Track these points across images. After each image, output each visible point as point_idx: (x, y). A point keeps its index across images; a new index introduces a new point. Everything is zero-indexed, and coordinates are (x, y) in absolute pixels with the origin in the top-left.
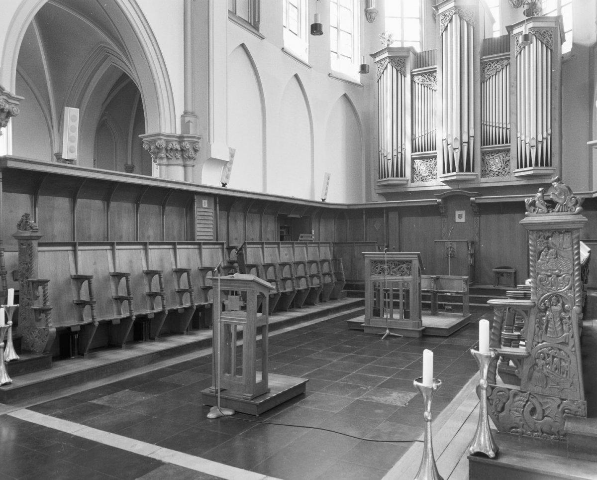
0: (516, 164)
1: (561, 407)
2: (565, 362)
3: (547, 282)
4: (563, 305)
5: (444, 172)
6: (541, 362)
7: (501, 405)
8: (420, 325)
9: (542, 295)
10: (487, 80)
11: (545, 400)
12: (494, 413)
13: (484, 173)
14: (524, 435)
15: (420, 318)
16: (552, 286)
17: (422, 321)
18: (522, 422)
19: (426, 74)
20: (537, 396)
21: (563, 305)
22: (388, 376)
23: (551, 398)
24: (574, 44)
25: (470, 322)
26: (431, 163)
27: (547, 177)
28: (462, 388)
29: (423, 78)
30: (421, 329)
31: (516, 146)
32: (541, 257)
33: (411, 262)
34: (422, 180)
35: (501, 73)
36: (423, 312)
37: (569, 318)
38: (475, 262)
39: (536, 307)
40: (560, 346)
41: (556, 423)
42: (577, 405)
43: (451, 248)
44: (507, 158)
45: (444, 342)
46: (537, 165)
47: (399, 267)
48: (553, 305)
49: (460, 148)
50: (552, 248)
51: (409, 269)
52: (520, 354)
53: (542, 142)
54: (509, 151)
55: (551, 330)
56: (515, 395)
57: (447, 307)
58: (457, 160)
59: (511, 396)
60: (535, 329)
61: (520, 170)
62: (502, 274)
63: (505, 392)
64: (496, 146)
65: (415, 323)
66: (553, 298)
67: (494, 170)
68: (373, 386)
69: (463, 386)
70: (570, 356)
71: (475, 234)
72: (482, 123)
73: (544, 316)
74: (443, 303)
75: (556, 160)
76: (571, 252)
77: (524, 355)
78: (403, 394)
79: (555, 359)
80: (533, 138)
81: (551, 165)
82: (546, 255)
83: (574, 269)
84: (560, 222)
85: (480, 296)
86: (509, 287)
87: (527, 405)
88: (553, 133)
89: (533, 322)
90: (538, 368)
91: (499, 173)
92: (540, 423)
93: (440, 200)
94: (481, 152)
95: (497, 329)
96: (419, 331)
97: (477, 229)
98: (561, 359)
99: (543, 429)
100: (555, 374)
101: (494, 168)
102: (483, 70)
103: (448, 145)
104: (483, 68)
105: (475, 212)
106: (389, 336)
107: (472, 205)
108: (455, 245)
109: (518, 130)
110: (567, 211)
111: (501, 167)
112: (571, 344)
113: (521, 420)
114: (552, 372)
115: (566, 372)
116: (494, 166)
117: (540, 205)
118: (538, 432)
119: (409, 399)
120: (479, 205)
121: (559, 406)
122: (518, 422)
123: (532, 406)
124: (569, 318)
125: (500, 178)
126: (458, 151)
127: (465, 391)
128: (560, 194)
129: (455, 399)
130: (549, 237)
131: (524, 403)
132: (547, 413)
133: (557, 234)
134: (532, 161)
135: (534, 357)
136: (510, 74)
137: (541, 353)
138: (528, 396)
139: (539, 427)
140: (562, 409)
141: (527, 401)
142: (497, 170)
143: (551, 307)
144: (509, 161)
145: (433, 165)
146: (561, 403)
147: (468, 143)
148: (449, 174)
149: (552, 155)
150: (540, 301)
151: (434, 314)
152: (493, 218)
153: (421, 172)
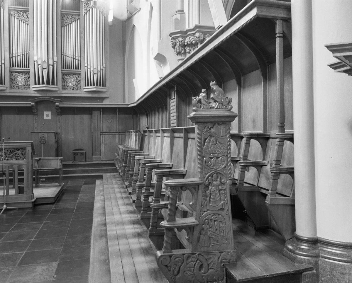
0: (85, 83)
4: (221, 179)
5: (35, 84)
6: (205, 227)
7: (177, 269)
9: (207, 174)
10: (65, 26)
11: (209, 257)
12: (171, 277)
13: (64, 87)
15: (32, 191)
16: (214, 166)
17: (33, 194)
18: (193, 279)
19: (21, 11)
20: (204, 255)
21: (221, 179)
22: (24, 250)
23: (213, 253)
24: (114, 17)
27: (103, 93)
28: (90, 246)
29: (19, 14)
30: (33, 200)
32: (206, 144)
33: (25, 149)
34: (19, 88)
35: (74, 23)
37: (225, 189)
38: (58, 146)
40: (220, 212)
41: (217, 272)
43: (43, 137)
45: (53, 207)
46: (97, 85)
47: (15, 153)
48: (214, 181)
49: (47, 68)
50: (214, 136)
54: (80, 74)
56: (188, 257)
57: (41, 179)
58: (45, 77)
59: (185, 259)
62: (77, 154)
63: (180, 258)
64: (76, 70)
65: (29, 196)
67: (71, 86)
68: (14, 265)
71: (58, 128)
72: (62, 53)
73: (208, 190)
78: (46, 267)
79: (215, 223)
80: (95, 68)
81: (105, 86)
84: (221, 116)
87: (197, 263)
88: (106, 67)
90: (204, 232)
91: (74, 88)
92: (206, 275)
93: (33, 104)
94: (62, 73)
97: (59, 125)
98: (219, 221)
101: (70, 84)
102: (62, 19)
103: (38, 65)
104: (62, 18)
105: (58, 113)
106: (6, 210)
107: (56, 108)
108: (46, 135)
109: (86, 62)
110: (223, 108)
111: (75, 84)
114: (214, 233)
115: (222, 231)
116: (70, 83)
117: (205, 102)
119: (55, 270)
120: (62, 108)
121: (219, 258)
123: (201, 263)
125: (74, 91)
126: (46, 70)
131: (195, 263)
132: (211, 266)
136: (80, 25)
141: (197, 260)
142: (72, 86)
144: (80, 81)
145: (27, 78)
146: (220, 255)
147: (53, 66)
149: (106, 80)
152: (70, 117)
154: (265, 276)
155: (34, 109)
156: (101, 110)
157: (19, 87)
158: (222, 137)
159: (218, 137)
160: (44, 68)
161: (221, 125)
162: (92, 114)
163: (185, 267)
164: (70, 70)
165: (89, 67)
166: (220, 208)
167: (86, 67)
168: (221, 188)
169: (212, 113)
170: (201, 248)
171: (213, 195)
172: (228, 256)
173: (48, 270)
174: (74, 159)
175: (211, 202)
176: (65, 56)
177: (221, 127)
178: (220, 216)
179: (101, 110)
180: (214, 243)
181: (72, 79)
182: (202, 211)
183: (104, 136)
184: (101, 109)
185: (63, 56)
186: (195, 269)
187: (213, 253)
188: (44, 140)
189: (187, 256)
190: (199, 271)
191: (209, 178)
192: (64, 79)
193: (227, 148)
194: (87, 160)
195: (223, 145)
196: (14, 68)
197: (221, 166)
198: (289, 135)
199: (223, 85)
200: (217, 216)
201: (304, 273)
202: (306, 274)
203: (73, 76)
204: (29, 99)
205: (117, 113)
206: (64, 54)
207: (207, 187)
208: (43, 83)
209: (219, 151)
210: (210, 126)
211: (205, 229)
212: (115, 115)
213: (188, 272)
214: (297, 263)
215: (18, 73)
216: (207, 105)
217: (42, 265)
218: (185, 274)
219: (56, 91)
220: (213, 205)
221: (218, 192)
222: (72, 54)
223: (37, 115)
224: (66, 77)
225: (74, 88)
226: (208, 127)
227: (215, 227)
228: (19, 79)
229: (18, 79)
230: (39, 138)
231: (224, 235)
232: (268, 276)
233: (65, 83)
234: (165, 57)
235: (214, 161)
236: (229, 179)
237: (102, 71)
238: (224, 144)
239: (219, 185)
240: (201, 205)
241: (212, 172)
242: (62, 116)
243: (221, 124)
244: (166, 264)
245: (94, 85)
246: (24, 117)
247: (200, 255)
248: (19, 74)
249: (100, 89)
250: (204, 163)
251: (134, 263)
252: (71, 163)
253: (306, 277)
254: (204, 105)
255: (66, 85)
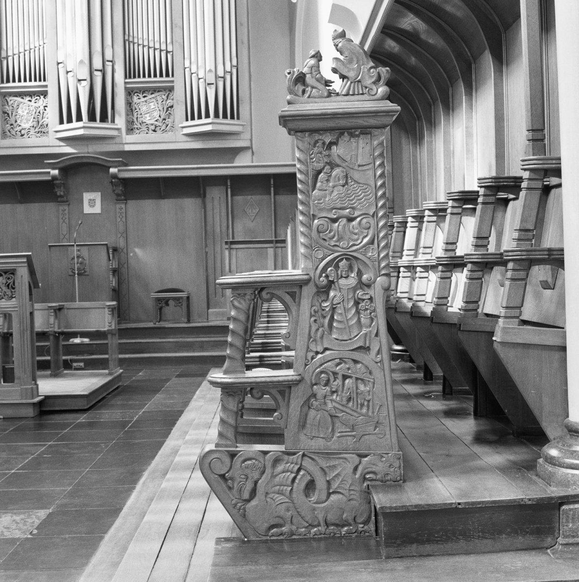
1: (360, 468)
2: (365, 386)
3: (330, 232)
4: (360, 274)
5: (61, 122)
6: (321, 391)
7: (249, 486)
8: (35, 392)
9: (323, 259)
11: (332, 463)
12: (236, 505)
14: (294, 537)
16: (339, 240)
17: (37, 385)
18: (289, 513)
20: (316, 458)
21: (360, 274)
25: (120, 384)
26: (37, 105)
28: (134, 488)
31: (184, 79)
32: (319, 184)
33: (13, 272)
36: (39, 373)
37: (371, 299)
38: (119, 283)
39: (311, 284)
40: (357, 356)
42: (386, 461)
43: (78, 257)
44: (169, 102)
45: (82, 418)
46: (217, 115)
48: (342, 277)
49: (89, 80)
50: (338, 166)
51: (11, 286)
52: (286, 378)
53: (224, 78)
54: (171, 89)
55: (340, 326)
56: (277, 461)
59: (269, 465)
60: (310, 327)
61: (190, 123)
62: (166, 301)
64: (155, 79)
65: (26, 389)
66: (341, 264)
67: (148, 122)
69: (136, 484)
70: (373, 370)
71: (119, 235)
72: (127, 38)
73: (326, 301)
74: (69, 357)
75: (244, 111)
76: (371, 173)
77: (292, 381)
78: (22, 516)
79: (347, 381)
80: (210, 71)
81: (238, 118)
82: (328, 181)
83: (377, 206)
85: (134, 341)
86: (178, 323)
87: (299, 477)
89: (308, 314)
90: (317, 403)
93: (56, 172)
95: (239, 335)
96: (34, 404)
98: (357, 379)
99: (328, 518)
100: (348, 411)
101: (147, 119)
103: (68, 72)
107: (112, 182)
108: (85, 252)
109: (186, 56)
110: (363, 94)
111: (160, 116)
112: (375, 348)
113: (288, 510)
114: (343, 405)
115: (366, 403)
118: (319, 525)
119: (37, 522)
120: (126, 182)
121: (356, 469)
122: (282, 513)
124: (371, 299)
126: (86, 85)
127: (140, 492)
128: (350, 61)
129: (125, 509)
130: (331, 144)
131: (293, 475)
132: (335, 486)
133: (346, 137)
134: (210, 111)
135: (309, 382)
137: (322, 372)
138: (299, 460)
139: (321, 517)
140: (361, 475)
141: (299, 470)
142: (152, 122)
143: (337, 281)
144: (172, 107)
145: (42, 108)
146: (360, 463)
147: (103, 72)
148: (70, 126)
149: (240, 102)
150: (318, 271)
151: (55, 375)
153: (18, 122)
154: (452, 504)
155: (58, 187)
156: (229, 184)
157: (23, 132)
158: (360, 168)
159: (351, 166)
160: (79, 80)
161: (358, 136)
162: (205, 196)
163: (267, 484)
164: (147, 79)
165: (194, 70)
166: (358, 345)
167: (187, 70)
168: (359, 296)
169: (329, 106)
170: (309, 440)
171: (340, 312)
172: (380, 464)
173: (25, 521)
174: (160, 314)
175: (335, 330)
176: (134, 44)
177: (358, 142)
178: (359, 366)
179: (229, 184)
180: (342, 432)
181: (152, 104)
182: (311, 351)
183: (234, 252)
184: (229, 181)
185: (134, 45)
186: (294, 490)
187: (340, 456)
188: (81, 263)
189: (274, 457)
190: (307, 496)
191: (329, 269)
192: (130, 106)
193: (376, 194)
194: (194, 316)
195: (365, 187)
196: (11, 84)
197: (359, 241)
198: (554, 162)
199: (473, 66)
200: (351, 364)
201: (565, 507)
202: (570, 510)
203: (153, 96)
204: (45, 161)
205: (272, 189)
206: (131, 39)
207: (324, 291)
208: (79, 118)
209: (354, 201)
210: (327, 141)
211: (319, 396)
212: (269, 196)
213: (277, 495)
214: (557, 486)
215: (20, 96)
216: (321, 86)
217: (15, 514)
218: (268, 500)
219: (112, 138)
220: (340, 338)
221: (352, 303)
222: (151, 38)
223: (67, 201)
224: (135, 99)
225: (158, 129)
226: (324, 143)
227: (346, 393)
228: (23, 112)
229: (20, 111)
230: (70, 259)
231: (370, 414)
232: (460, 506)
233: (135, 114)
234: (353, 13)
235: (340, 227)
236: (383, 272)
237: (228, 77)
238: (368, 185)
239: (355, 289)
240: (306, 336)
241: (336, 254)
242: (129, 202)
243: (357, 133)
244: (222, 473)
245: (207, 116)
246: (35, 208)
247: (305, 458)
248: (23, 98)
249: (226, 125)
250: (314, 234)
251: (205, 510)
252: (151, 326)
253: (570, 516)
254: (313, 87)
255: (135, 120)
